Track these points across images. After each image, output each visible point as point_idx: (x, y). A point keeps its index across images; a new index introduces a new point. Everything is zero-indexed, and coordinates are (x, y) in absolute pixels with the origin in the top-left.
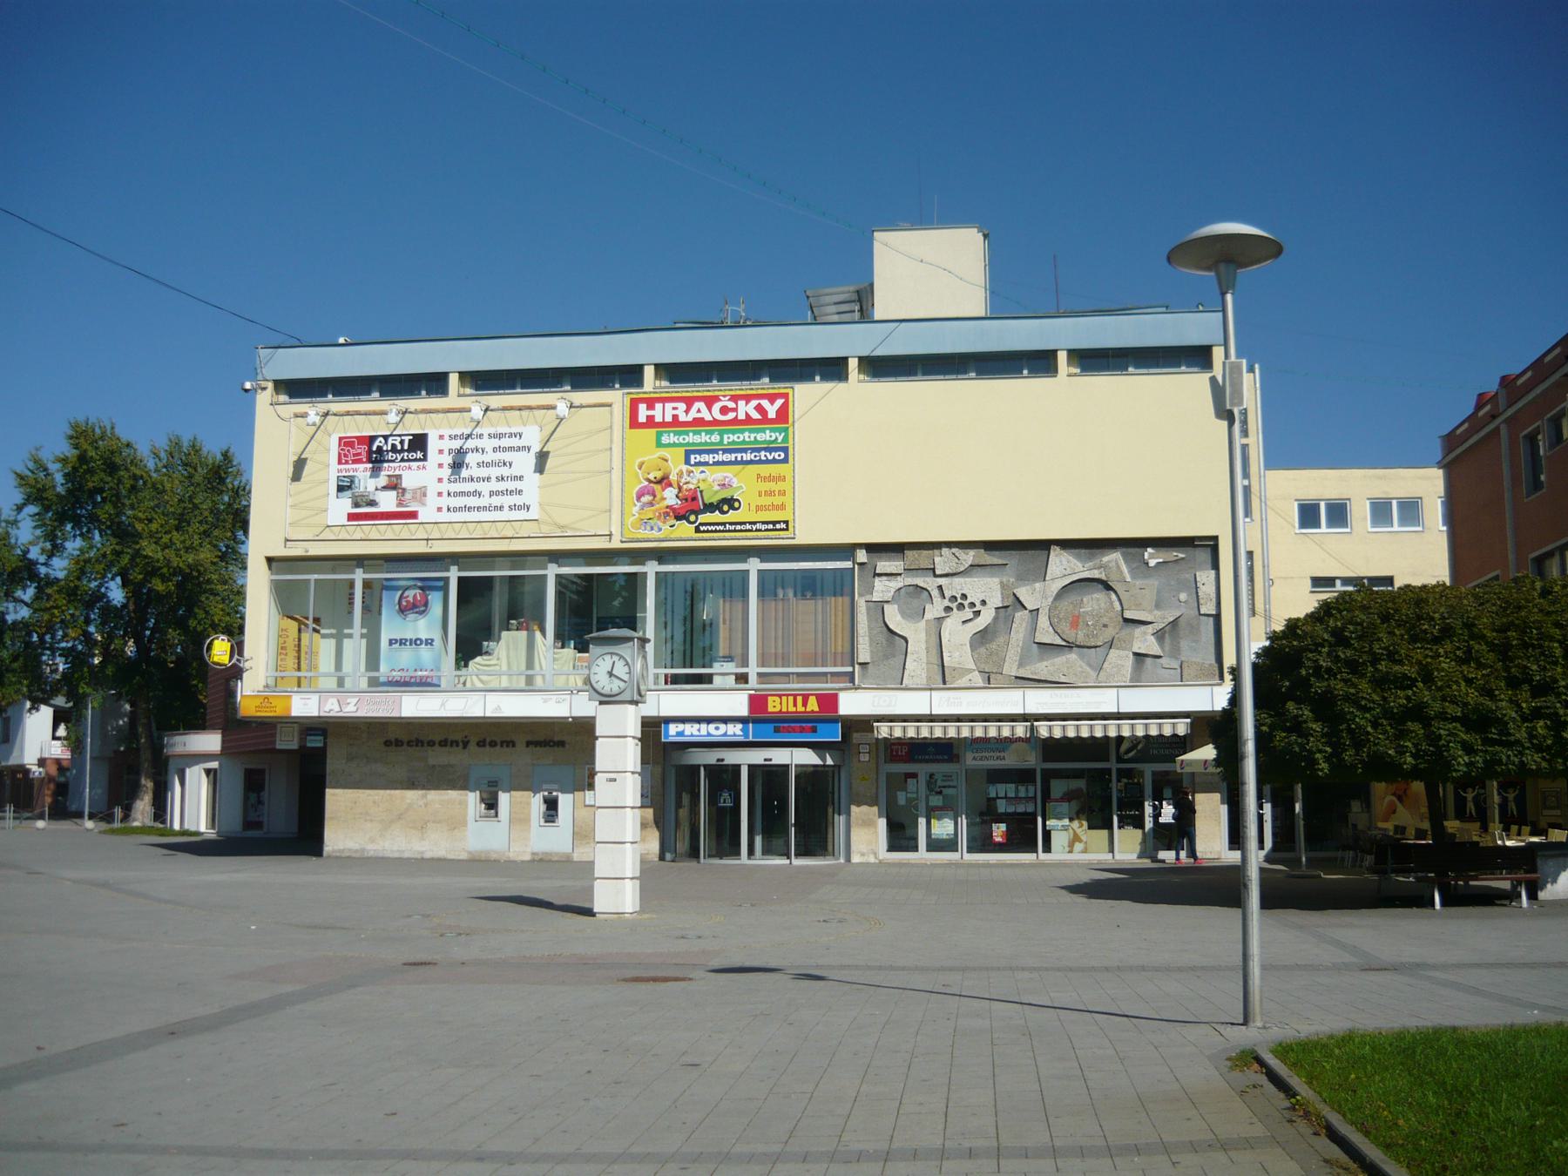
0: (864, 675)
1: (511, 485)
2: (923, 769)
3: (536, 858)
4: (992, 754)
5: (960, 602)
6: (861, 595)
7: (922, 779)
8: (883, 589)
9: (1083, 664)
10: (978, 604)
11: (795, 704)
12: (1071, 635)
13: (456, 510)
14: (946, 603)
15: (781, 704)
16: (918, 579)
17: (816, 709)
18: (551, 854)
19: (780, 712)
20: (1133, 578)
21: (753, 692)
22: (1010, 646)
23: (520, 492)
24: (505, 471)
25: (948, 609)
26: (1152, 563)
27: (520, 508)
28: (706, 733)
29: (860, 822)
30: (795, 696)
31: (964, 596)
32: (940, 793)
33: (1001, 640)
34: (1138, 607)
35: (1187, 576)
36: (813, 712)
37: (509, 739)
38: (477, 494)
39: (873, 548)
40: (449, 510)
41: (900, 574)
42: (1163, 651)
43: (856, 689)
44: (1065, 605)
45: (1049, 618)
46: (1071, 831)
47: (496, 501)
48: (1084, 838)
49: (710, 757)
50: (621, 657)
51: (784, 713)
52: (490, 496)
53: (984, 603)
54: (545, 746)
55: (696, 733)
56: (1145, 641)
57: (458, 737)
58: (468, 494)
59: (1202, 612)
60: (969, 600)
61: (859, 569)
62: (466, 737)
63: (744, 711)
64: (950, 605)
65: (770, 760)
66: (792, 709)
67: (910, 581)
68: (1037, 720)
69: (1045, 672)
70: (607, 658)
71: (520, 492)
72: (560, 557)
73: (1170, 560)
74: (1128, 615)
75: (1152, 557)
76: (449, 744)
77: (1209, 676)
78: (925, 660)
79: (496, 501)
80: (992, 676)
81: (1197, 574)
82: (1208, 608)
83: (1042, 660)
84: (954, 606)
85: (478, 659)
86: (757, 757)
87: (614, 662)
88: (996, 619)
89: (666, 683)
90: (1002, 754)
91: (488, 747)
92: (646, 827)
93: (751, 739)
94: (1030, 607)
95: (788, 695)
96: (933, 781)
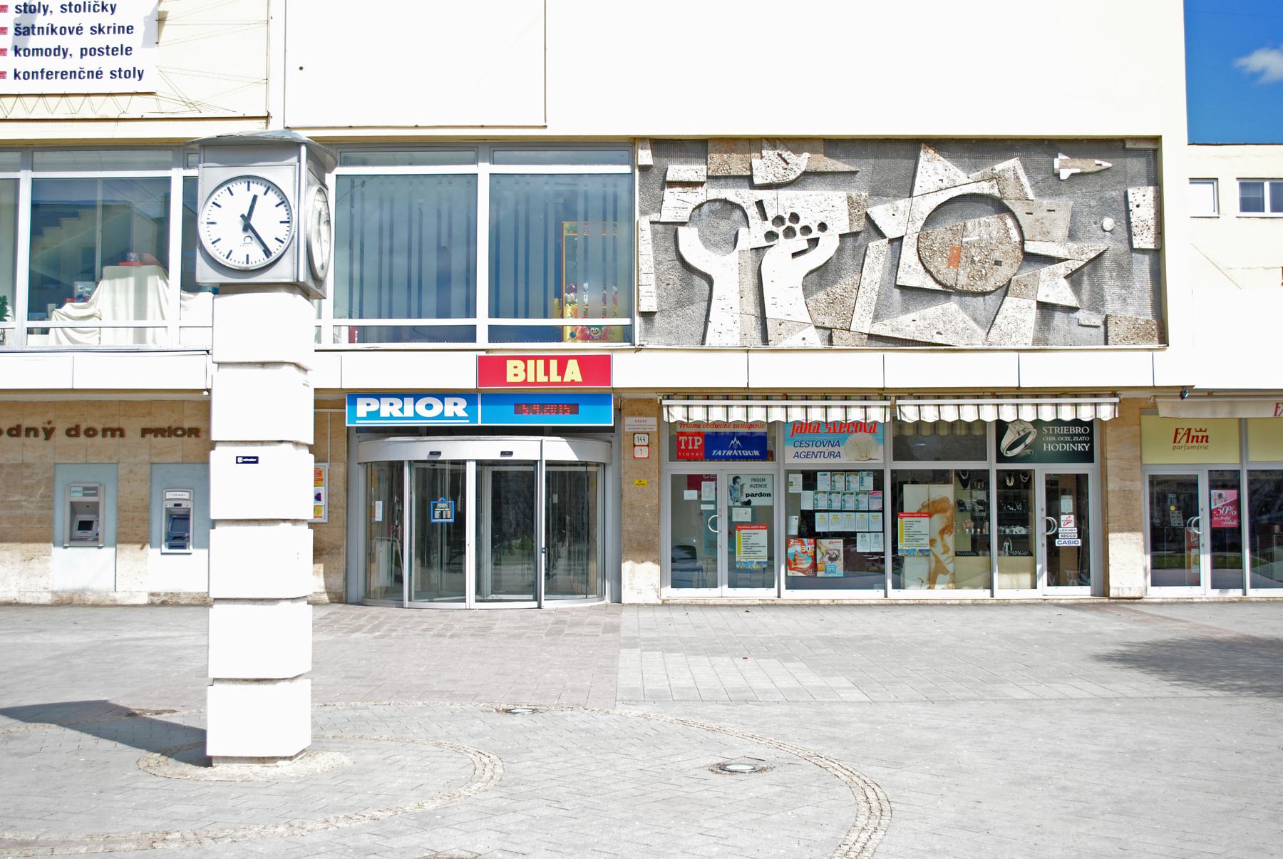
0: (647, 330)
1: (114, 40)
2: (724, 470)
3: (157, 600)
4: (822, 449)
5: (788, 225)
6: (643, 213)
7: (724, 483)
8: (676, 205)
9: (967, 318)
10: (814, 228)
11: (547, 372)
12: (948, 275)
13: (27, 75)
14: (769, 226)
15: (526, 370)
16: (728, 190)
17: (578, 378)
18: (178, 595)
19: (525, 382)
20: (1038, 195)
21: (483, 354)
22: (861, 290)
23: (128, 51)
24: (105, 19)
25: (771, 236)
26: (1065, 174)
27: (128, 74)
28: (412, 415)
29: (635, 545)
30: (547, 360)
31: (795, 218)
32: (748, 503)
33: (848, 281)
34: (1046, 236)
35: (1114, 193)
36: (573, 382)
37: (115, 425)
38: (61, 52)
39: (666, 146)
40: (16, 75)
41: (702, 184)
42: (1080, 300)
43: (638, 350)
44: (940, 232)
45: (918, 251)
46: (932, 558)
47: (91, 63)
48: (950, 567)
49: (420, 450)
50: (270, 186)
51: (531, 384)
52: (82, 55)
53: (823, 227)
54: (169, 436)
55: (397, 414)
56: (1053, 287)
57: (38, 422)
58: (47, 52)
59: (1136, 246)
60: (802, 223)
61: (641, 176)
62: (49, 423)
63: (467, 378)
64: (774, 229)
65: (511, 453)
66: (542, 378)
67: (715, 193)
68: (899, 398)
69: (912, 327)
70: (239, 188)
71: (128, 51)
72: (193, 152)
73: (1089, 170)
74: (1030, 247)
75: (1065, 166)
76: (23, 433)
77: (1146, 336)
78: (737, 309)
79: (91, 63)
80: (836, 333)
81: (1130, 191)
82: (1145, 240)
83: (906, 310)
84: (780, 230)
85: (68, 308)
86: (490, 449)
87: (255, 198)
88: (840, 250)
89: (351, 340)
90: (836, 449)
91: (83, 438)
92: (321, 555)
93: (480, 424)
94: (891, 232)
95: (536, 358)
96: (737, 486)
